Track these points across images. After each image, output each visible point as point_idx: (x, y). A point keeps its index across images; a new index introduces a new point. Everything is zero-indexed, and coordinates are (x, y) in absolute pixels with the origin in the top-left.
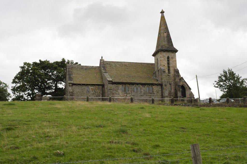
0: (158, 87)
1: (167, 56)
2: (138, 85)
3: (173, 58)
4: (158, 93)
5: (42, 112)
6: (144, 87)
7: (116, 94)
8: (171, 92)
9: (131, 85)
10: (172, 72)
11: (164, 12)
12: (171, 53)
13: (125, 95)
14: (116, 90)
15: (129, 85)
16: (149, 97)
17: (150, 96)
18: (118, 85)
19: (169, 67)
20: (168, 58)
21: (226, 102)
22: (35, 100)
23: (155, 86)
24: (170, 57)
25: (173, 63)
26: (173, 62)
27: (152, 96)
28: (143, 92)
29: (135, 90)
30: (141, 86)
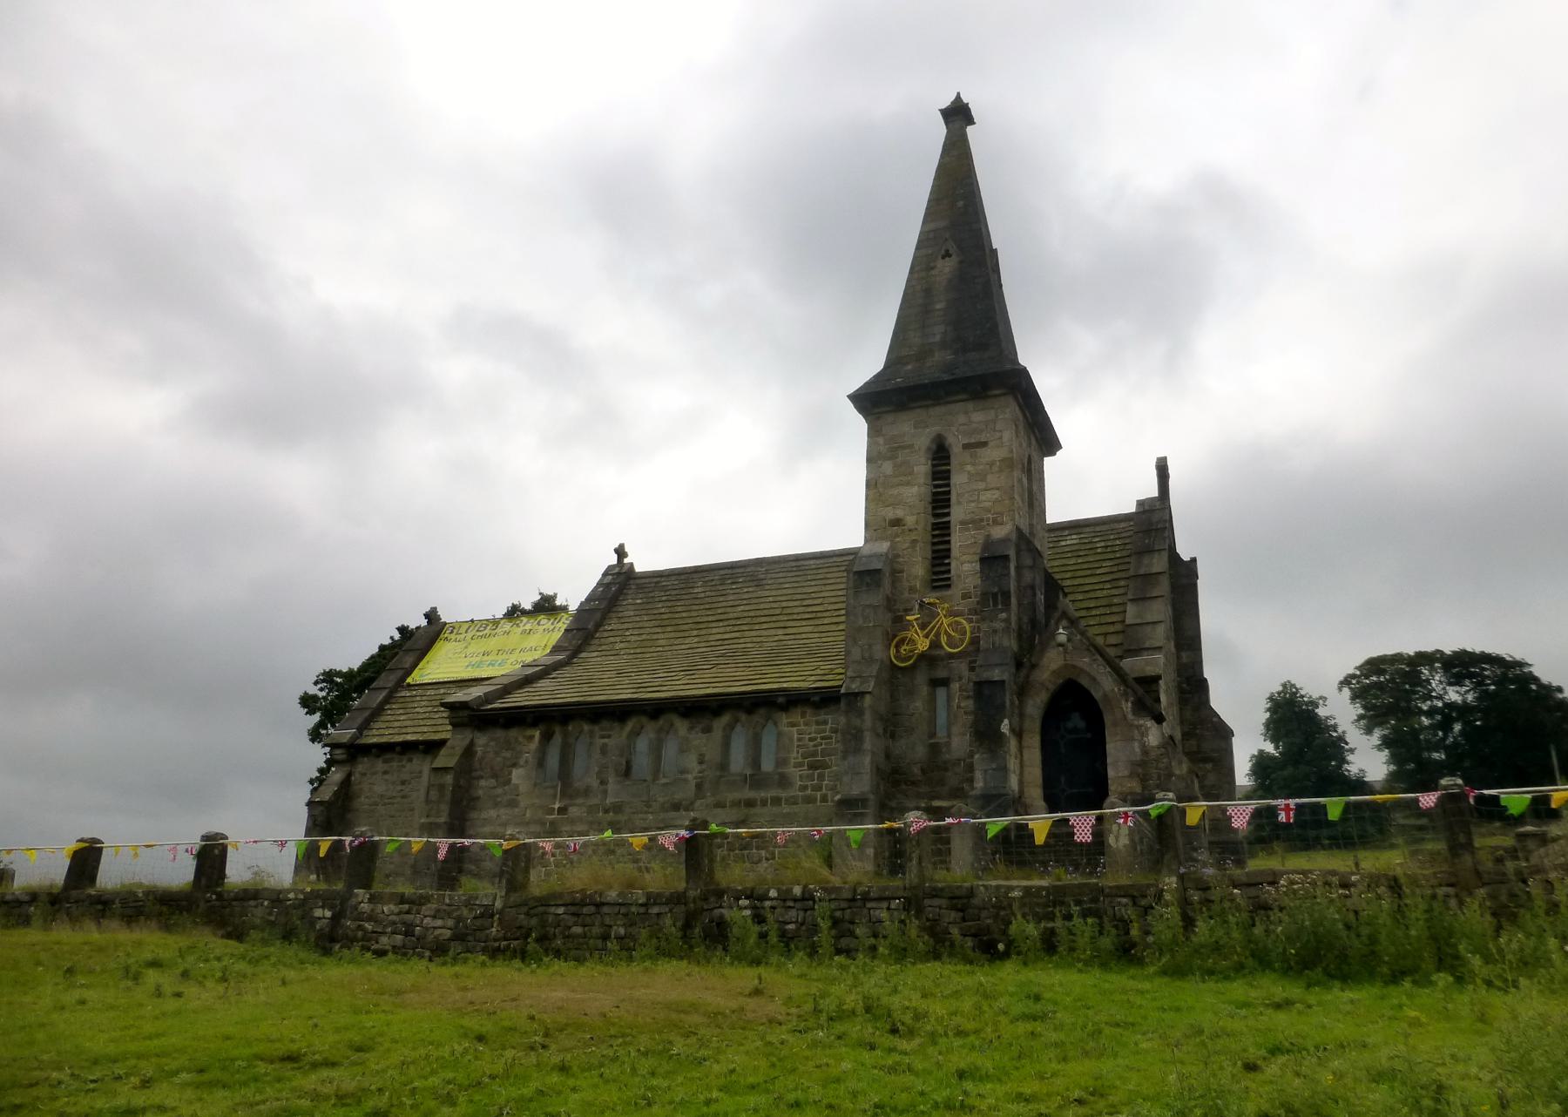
0: (822, 717)
1: (923, 441)
2: (661, 722)
3: (984, 444)
4: (821, 777)
5: (1016, 711)
6: (707, 730)
7: (496, 805)
8: (142, 918)
9: (605, 723)
10: (966, 567)
11: (311, 779)
12: (970, 405)
13: (551, 811)
14: (495, 776)
15: (596, 728)
16: (734, 814)
17: (750, 804)
18: (513, 733)
19: (941, 531)
20: (940, 454)
21: (712, 887)
22: (238, 935)
23: (796, 716)
24: (955, 443)
25: (981, 485)
26: (983, 479)
27: (764, 803)
28: (690, 777)
29: (642, 761)
30: (681, 726)
